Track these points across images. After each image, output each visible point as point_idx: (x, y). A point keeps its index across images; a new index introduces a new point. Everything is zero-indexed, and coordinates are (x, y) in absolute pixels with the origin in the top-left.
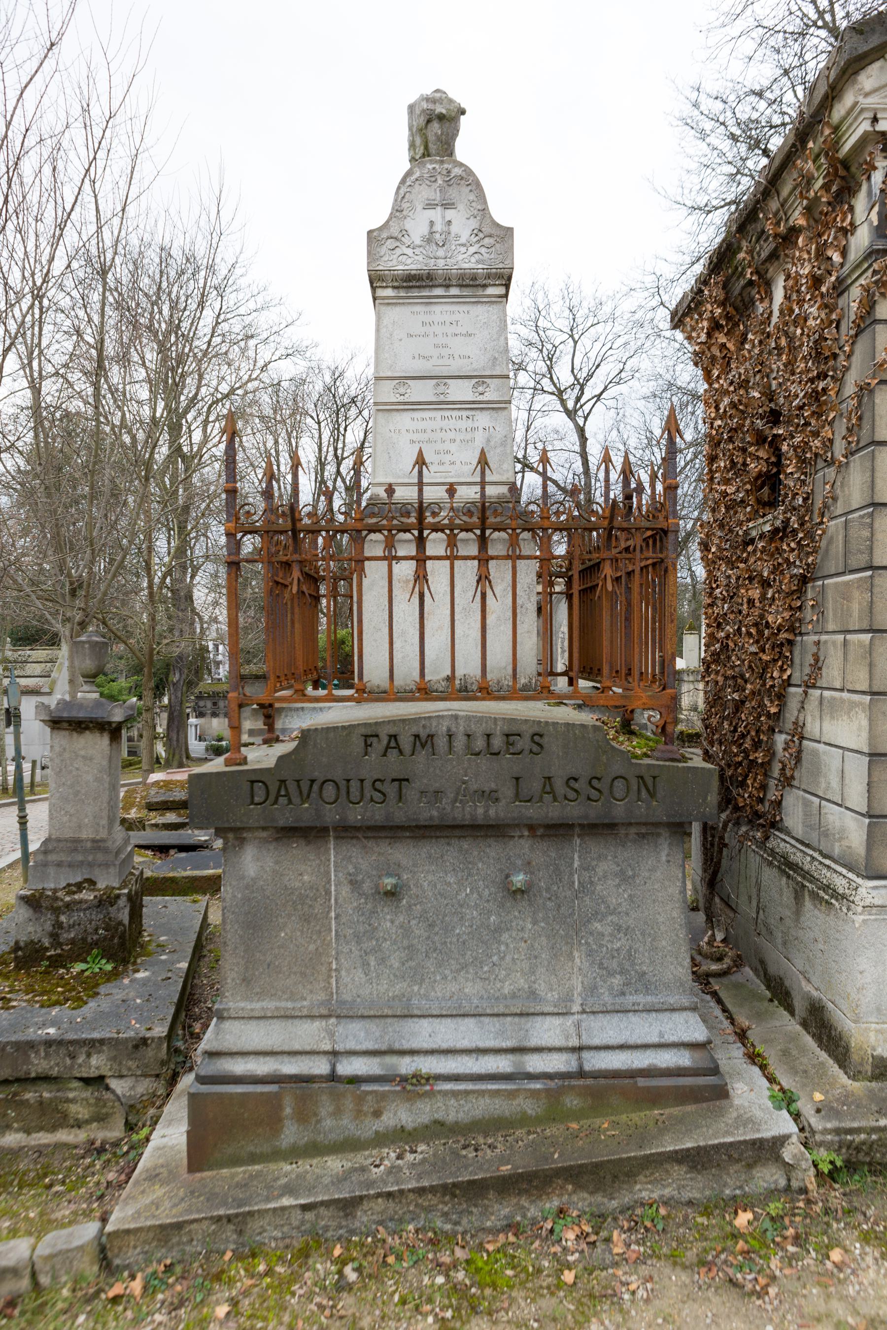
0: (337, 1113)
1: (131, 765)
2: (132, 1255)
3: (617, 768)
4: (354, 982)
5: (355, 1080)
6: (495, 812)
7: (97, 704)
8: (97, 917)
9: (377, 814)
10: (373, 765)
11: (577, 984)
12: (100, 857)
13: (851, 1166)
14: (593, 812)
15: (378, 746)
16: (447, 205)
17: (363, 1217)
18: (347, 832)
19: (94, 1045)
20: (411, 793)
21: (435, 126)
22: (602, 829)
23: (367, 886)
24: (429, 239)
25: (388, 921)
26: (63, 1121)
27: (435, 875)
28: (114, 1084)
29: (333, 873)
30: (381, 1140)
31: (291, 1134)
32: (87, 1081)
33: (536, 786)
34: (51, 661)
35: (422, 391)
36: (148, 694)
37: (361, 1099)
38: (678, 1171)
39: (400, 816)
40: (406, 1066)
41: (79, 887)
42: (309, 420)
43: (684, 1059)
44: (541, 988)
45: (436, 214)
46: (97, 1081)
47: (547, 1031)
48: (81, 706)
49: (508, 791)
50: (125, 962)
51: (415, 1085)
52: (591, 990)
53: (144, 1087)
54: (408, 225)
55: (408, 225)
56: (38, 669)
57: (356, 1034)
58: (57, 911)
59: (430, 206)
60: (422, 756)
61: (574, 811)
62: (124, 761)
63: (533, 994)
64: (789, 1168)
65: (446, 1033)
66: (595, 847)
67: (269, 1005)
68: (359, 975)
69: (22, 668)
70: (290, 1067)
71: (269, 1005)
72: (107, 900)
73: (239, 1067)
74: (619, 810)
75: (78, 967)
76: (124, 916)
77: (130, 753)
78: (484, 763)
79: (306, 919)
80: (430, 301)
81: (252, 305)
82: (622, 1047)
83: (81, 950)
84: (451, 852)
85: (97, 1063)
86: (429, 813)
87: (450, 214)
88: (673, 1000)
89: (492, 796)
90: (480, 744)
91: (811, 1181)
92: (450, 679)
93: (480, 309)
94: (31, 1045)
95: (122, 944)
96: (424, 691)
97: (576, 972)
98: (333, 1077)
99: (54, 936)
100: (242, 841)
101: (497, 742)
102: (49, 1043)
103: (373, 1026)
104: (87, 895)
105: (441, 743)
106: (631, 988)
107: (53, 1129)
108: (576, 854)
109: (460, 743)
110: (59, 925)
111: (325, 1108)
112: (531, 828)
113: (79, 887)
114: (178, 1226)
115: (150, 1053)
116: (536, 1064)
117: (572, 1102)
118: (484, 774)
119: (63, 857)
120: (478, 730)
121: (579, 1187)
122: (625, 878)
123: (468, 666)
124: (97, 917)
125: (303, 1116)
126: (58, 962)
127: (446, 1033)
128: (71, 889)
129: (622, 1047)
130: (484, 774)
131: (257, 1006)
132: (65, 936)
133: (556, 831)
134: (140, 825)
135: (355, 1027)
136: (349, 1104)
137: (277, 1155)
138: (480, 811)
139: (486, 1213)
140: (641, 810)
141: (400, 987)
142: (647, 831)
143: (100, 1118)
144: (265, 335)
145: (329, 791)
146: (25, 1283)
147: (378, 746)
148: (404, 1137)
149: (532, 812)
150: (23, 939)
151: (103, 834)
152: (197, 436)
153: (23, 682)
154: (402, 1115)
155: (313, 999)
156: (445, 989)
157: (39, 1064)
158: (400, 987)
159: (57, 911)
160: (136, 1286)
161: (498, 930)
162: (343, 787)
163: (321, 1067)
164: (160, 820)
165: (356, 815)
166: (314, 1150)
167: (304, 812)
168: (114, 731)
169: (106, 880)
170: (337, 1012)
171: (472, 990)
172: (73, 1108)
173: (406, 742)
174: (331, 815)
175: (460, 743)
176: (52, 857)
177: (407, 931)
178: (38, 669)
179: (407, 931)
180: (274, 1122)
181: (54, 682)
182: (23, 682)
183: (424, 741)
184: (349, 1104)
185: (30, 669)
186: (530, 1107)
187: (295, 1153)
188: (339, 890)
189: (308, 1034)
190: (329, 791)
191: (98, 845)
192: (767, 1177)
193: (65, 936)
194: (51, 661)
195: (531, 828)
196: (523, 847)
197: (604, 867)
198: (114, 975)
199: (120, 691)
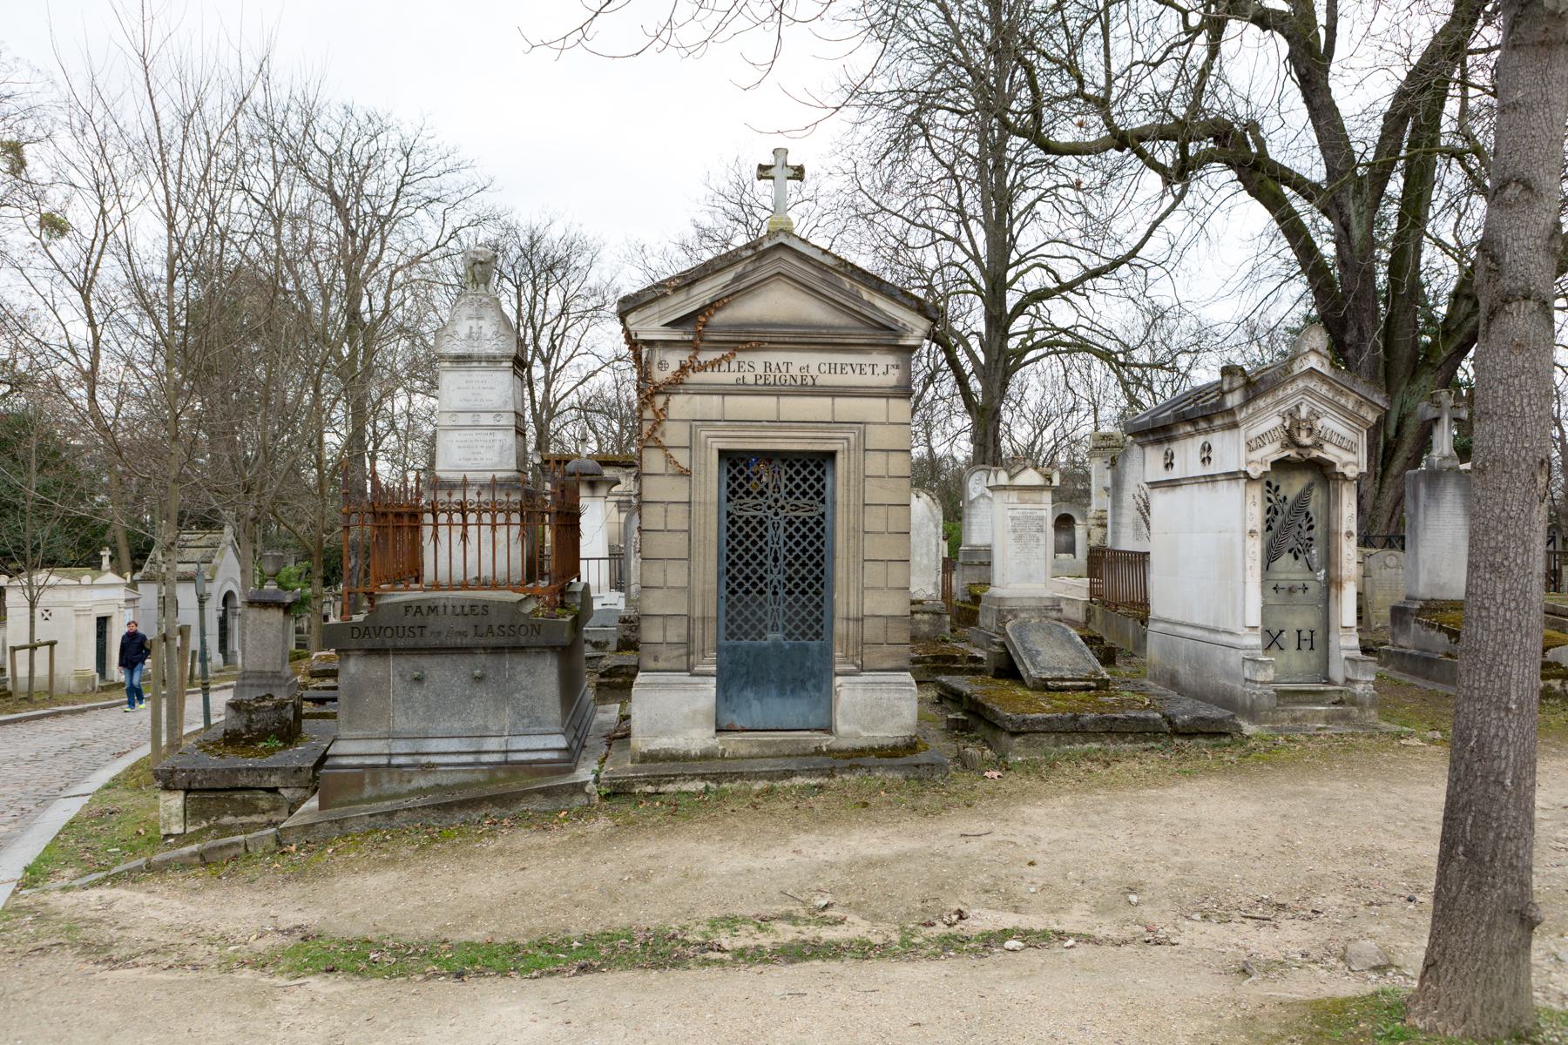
0: (391, 781)
1: (299, 658)
2: (291, 838)
3: (522, 622)
4: (401, 722)
5: (399, 766)
6: (466, 641)
7: (276, 592)
8: (274, 716)
9: (411, 643)
10: (409, 620)
11: (507, 722)
12: (277, 681)
13: (615, 794)
14: (511, 641)
15: (412, 611)
16: (479, 318)
17: (397, 820)
18: (398, 651)
19: (272, 771)
20: (427, 633)
21: (478, 267)
22: (517, 649)
23: (408, 677)
24: (470, 336)
25: (417, 693)
26: (255, 810)
27: (438, 670)
28: (283, 791)
29: (392, 670)
30: (411, 793)
31: (368, 791)
32: (268, 790)
33: (485, 630)
34: (213, 546)
35: (465, 419)
36: (318, 582)
37: (401, 775)
38: (539, 797)
39: (421, 644)
40: (424, 760)
41: (263, 698)
42: (506, 284)
43: (555, 755)
44: (490, 724)
45: (473, 323)
46: (274, 790)
47: (492, 744)
48: (266, 593)
49: (472, 632)
50: (291, 744)
51: (430, 767)
52: (514, 725)
53: (300, 793)
54: (458, 328)
55: (458, 328)
56: (197, 554)
57: (401, 746)
58: (250, 712)
59: (470, 318)
60: (432, 616)
61: (502, 641)
62: (292, 653)
63: (486, 727)
64: (588, 795)
65: (444, 745)
66: (516, 658)
67: (360, 733)
68: (404, 719)
69: (180, 554)
70: (369, 761)
71: (360, 733)
72: (281, 706)
73: (344, 761)
74: (523, 641)
75: (261, 745)
76: (291, 716)
77: (298, 646)
78: (460, 619)
79: (379, 693)
80: (469, 370)
81: (441, 167)
82: (526, 751)
83: (264, 735)
84: (448, 661)
85: (274, 780)
86: (435, 642)
87: (481, 323)
88: (551, 729)
89: (464, 634)
90: (458, 610)
91: (596, 799)
92: (478, 579)
93: (499, 374)
94: (239, 770)
95: (289, 732)
96: (465, 585)
97: (507, 717)
98: (389, 765)
99: (248, 727)
100: (348, 656)
101: (467, 609)
102: (248, 769)
103: (409, 742)
104: (269, 703)
105: (441, 610)
106: (533, 724)
107: (249, 814)
108: (507, 661)
109: (449, 610)
110: (251, 720)
111: (385, 779)
112: (485, 648)
113: (263, 698)
114: (313, 825)
115: (303, 775)
116: (485, 758)
117: (501, 775)
118: (461, 624)
119: (254, 681)
120: (458, 604)
121: (495, 805)
122: (530, 673)
123: (487, 572)
124: (274, 716)
125: (374, 783)
126: (250, 742)
127: (444, 745)
128: (257, 700)
129: (526, 751)
130: (461, 624)
131: (354, 734)
132: (254, 727)
133: (497, 650)
134: (305, 686)
135: (402, 743)
136: (396, 776)
137: (362, 801)
138: (459, 641)
139: (453, 818)
140: (533, 640)
141: (423, 724)
142: (541, 650)
143: (275, 809)
144: (454, 199)
145: (389, 632)
146: (242, 850)
147: (412, 611)
148: (421, 791)
149: (482, 641)
150: (229, 728)
151: (278, 668)
152: (379, 303)
153: (181, 568)
154: (421, 782)
155: (382, 730)
156: (444, 726)
157: (243, 780)
158: (423, 724)
159: (250, 712)
160: (293, 848)
161: (470, 697)
162: (395, 631)
163: (384, 761)
164: (321, 684)
165: (401, 643)
166: (380, 798)
167: (377, 642)
168: (287, 609)
169: (280, 695)
170: (392, 736)
171: (457, 726)
172: (261, 803)
173: (424, 610)
174: (389, 643)
175: (449, 610)
176: (248, 682)
177: (426, 697)
178: (197, 554)
179: (426, 697)
180: (361, 786)
181: (215, 569)
182: (181, 568)
183: (433, 609)
184: (396, 776)
185: (189, 554)
186: (481, 777)
187: (370, 800)
188: (395, 679)
189: (378, 746)
190: (389, 632)
191: (275, 675)
192: (579, 800)
193: (254, 727)
194: (213, 546)
195: (485, 648)
196: (482, 659)
197: (519, 668)
198: (284, 747)
199: (288, 578)
